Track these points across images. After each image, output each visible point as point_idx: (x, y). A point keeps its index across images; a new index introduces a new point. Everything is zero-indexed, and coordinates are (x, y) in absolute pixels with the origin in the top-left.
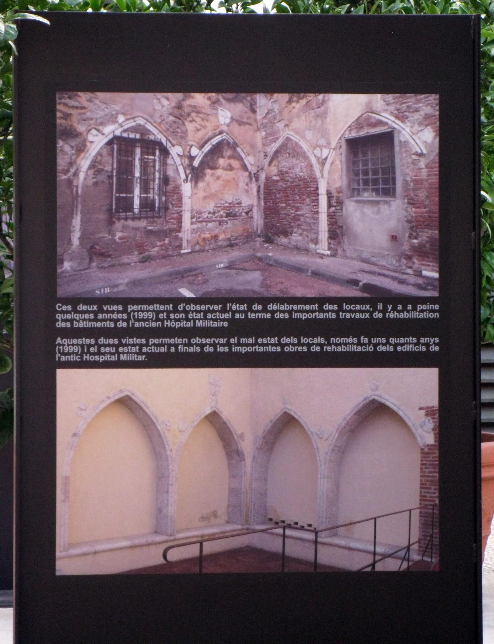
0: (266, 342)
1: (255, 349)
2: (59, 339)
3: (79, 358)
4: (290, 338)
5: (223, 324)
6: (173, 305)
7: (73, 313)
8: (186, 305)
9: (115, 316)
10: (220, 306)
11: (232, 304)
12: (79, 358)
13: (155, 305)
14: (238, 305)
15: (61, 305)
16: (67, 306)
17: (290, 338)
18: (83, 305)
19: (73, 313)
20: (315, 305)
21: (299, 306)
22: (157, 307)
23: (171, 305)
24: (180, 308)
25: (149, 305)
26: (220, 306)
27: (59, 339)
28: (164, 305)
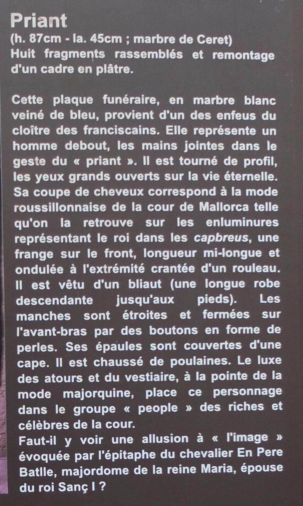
3: (273, 102)
5: (149, 101)
6: (203, 51)
7: (79, 111)
8: (33, 221)
11: (106, 452)
12: (273, 102)
13: (30, 97)
14: (233, 174)
15: (203, 36)
16: (162, 159)
19: (79, 111)
20: (105, 313)
21: (149, 53)
22: (32, 100)
26: (111, 330)
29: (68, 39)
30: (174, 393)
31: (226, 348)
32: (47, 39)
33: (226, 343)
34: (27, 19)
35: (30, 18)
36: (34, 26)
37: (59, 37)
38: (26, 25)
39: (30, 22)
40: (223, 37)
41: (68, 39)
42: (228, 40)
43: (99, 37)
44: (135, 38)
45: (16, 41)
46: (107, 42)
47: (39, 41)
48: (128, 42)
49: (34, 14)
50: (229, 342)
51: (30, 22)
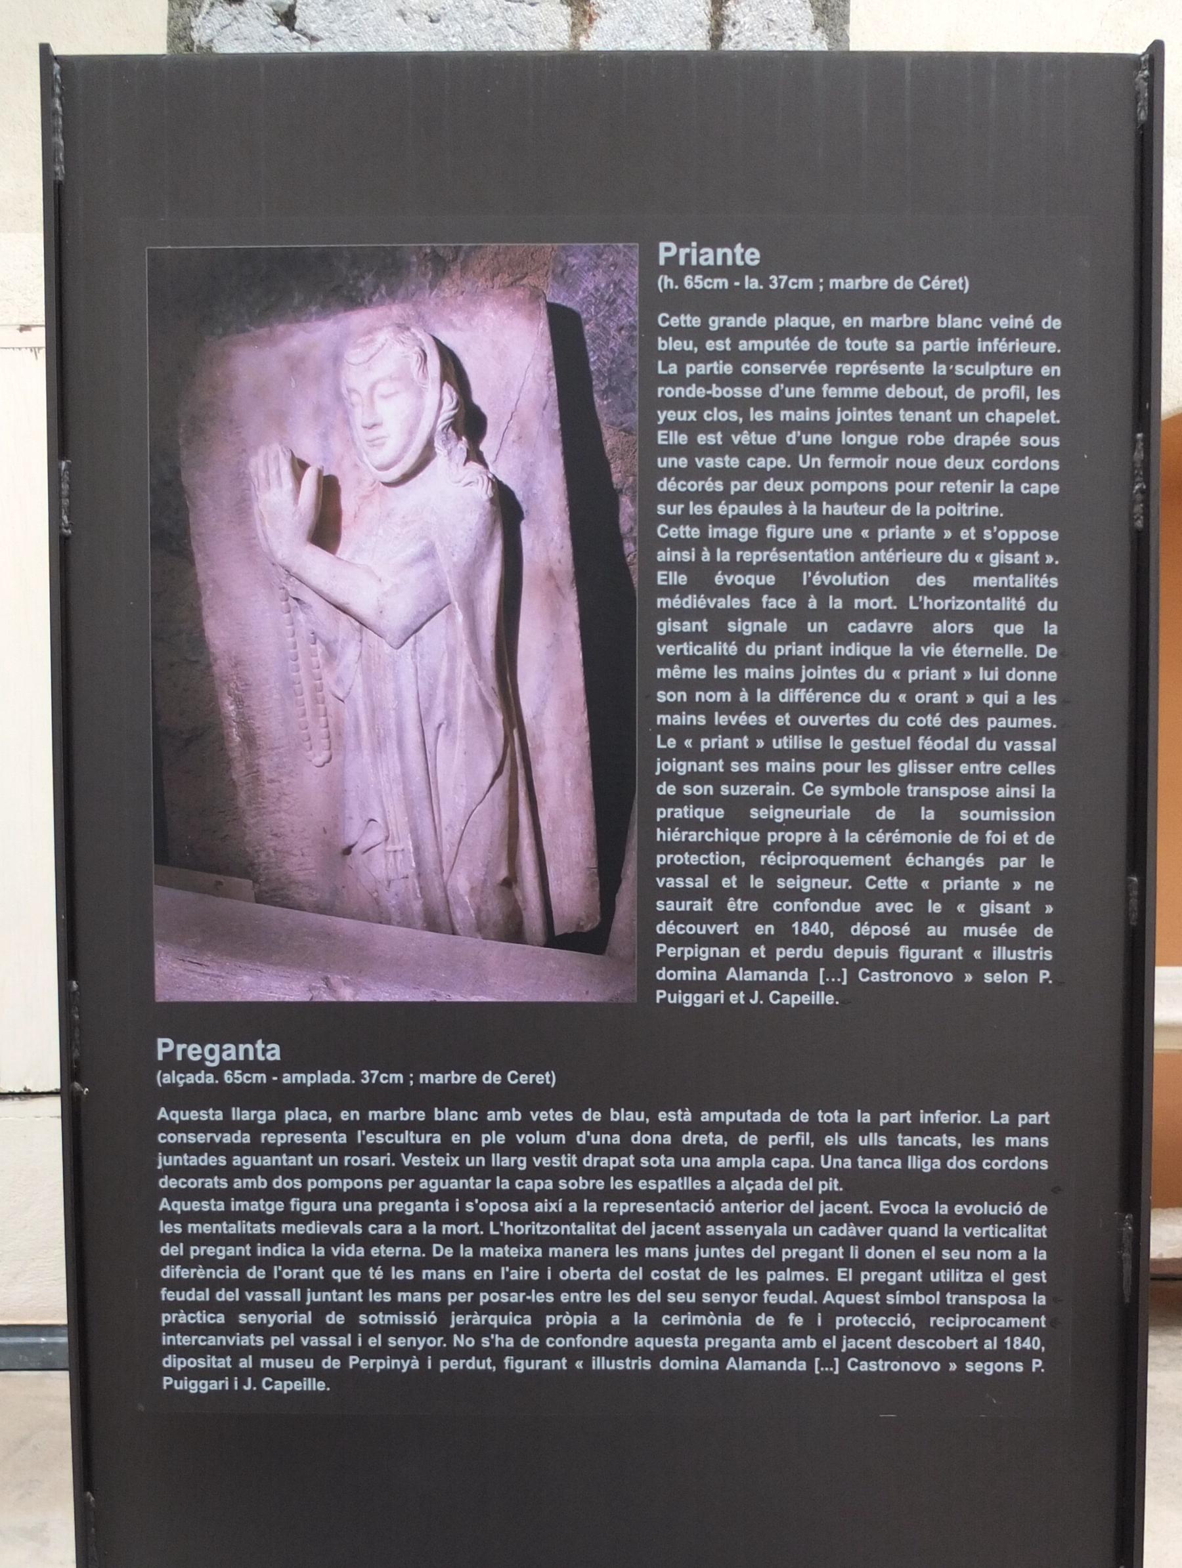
0: (428, 1163)
1: (595, 1275)
2: (163, 1109)
4: (445, 1157)
9: (579, 1341)
10: (1023, 859)
11: (813, 574)
13: (682, 317)
15: (811, 785)
17: (445, 1157)
18: (961, 717)
23: (960, 950)
24: (581, 1139)
25: (795, 809)
26: (1023, 859)
27: (163, 1109)
28: (1050, 367)
29: (737, 284)
30: (1019, 629)
31: (848, 724)
32: (793, 284)
33: (848, 717)
34: (683, 252)
35: (688, 250)
36: (694, 262)
37: (811, 281)
38: (682, 262)
39: (688, 256)
40: (957, 279)
41: (737, 284)
42: (964, 285)
43: (696, 281)
44: (832, 281)
45: (666, 287)
46: (707, 287)
47: (782, 286)
48: (821, 288)
49: (694, 244)
50: (852, 715)
51: (688, 256)
